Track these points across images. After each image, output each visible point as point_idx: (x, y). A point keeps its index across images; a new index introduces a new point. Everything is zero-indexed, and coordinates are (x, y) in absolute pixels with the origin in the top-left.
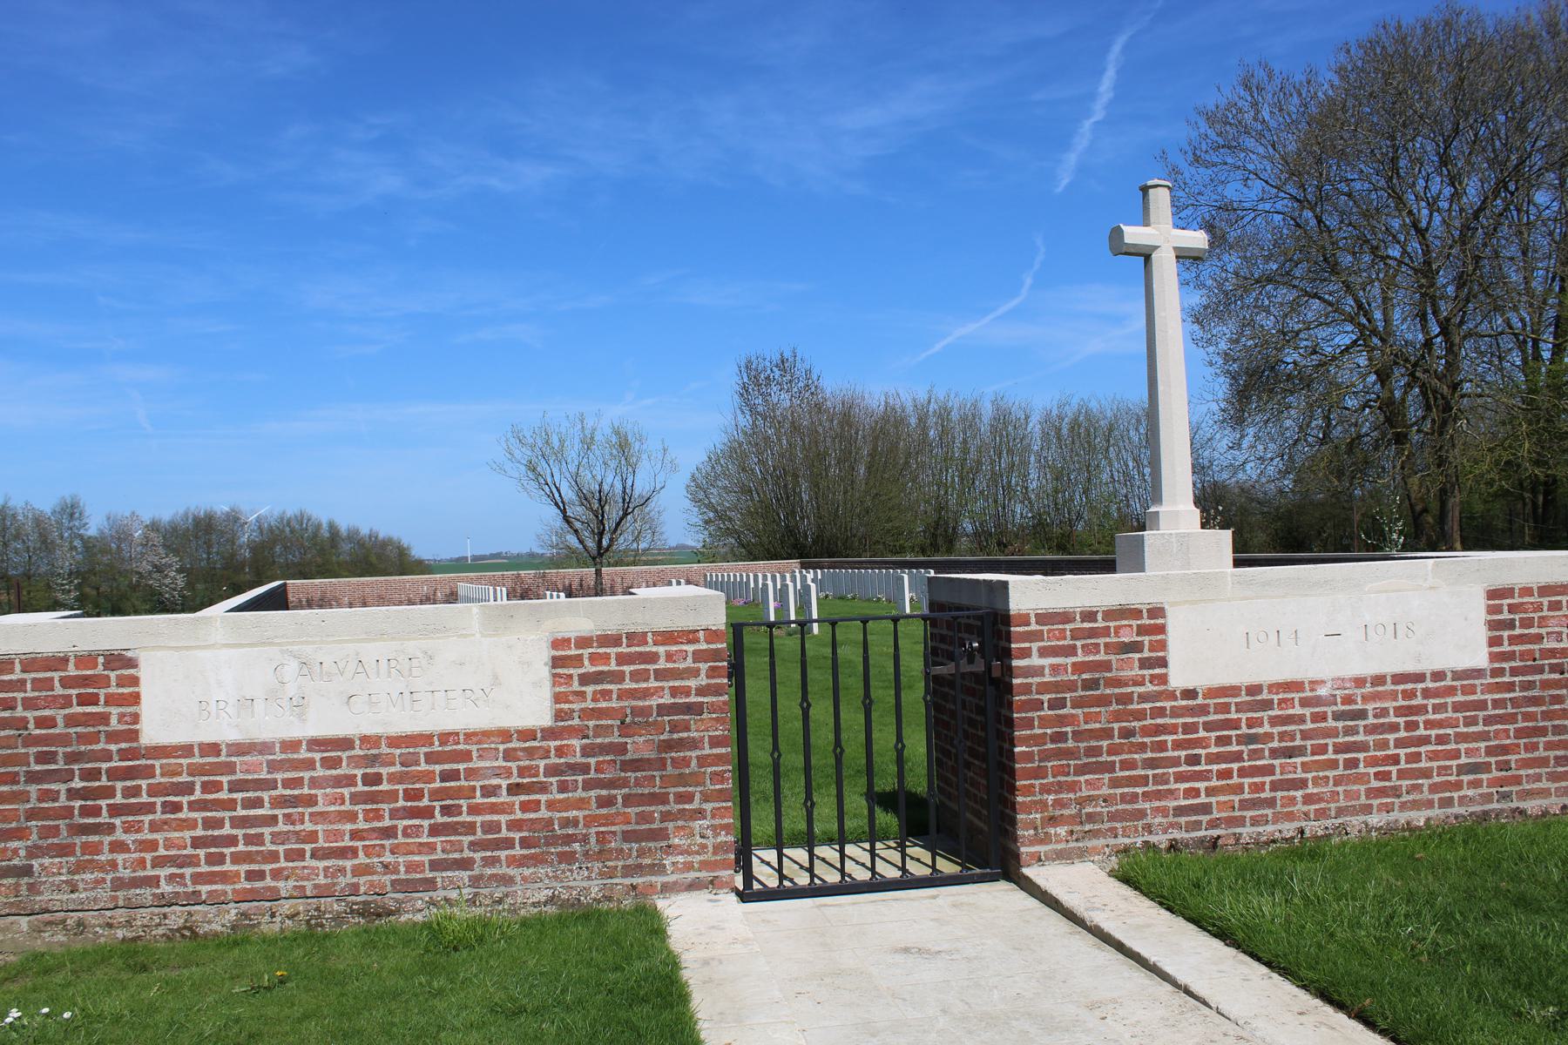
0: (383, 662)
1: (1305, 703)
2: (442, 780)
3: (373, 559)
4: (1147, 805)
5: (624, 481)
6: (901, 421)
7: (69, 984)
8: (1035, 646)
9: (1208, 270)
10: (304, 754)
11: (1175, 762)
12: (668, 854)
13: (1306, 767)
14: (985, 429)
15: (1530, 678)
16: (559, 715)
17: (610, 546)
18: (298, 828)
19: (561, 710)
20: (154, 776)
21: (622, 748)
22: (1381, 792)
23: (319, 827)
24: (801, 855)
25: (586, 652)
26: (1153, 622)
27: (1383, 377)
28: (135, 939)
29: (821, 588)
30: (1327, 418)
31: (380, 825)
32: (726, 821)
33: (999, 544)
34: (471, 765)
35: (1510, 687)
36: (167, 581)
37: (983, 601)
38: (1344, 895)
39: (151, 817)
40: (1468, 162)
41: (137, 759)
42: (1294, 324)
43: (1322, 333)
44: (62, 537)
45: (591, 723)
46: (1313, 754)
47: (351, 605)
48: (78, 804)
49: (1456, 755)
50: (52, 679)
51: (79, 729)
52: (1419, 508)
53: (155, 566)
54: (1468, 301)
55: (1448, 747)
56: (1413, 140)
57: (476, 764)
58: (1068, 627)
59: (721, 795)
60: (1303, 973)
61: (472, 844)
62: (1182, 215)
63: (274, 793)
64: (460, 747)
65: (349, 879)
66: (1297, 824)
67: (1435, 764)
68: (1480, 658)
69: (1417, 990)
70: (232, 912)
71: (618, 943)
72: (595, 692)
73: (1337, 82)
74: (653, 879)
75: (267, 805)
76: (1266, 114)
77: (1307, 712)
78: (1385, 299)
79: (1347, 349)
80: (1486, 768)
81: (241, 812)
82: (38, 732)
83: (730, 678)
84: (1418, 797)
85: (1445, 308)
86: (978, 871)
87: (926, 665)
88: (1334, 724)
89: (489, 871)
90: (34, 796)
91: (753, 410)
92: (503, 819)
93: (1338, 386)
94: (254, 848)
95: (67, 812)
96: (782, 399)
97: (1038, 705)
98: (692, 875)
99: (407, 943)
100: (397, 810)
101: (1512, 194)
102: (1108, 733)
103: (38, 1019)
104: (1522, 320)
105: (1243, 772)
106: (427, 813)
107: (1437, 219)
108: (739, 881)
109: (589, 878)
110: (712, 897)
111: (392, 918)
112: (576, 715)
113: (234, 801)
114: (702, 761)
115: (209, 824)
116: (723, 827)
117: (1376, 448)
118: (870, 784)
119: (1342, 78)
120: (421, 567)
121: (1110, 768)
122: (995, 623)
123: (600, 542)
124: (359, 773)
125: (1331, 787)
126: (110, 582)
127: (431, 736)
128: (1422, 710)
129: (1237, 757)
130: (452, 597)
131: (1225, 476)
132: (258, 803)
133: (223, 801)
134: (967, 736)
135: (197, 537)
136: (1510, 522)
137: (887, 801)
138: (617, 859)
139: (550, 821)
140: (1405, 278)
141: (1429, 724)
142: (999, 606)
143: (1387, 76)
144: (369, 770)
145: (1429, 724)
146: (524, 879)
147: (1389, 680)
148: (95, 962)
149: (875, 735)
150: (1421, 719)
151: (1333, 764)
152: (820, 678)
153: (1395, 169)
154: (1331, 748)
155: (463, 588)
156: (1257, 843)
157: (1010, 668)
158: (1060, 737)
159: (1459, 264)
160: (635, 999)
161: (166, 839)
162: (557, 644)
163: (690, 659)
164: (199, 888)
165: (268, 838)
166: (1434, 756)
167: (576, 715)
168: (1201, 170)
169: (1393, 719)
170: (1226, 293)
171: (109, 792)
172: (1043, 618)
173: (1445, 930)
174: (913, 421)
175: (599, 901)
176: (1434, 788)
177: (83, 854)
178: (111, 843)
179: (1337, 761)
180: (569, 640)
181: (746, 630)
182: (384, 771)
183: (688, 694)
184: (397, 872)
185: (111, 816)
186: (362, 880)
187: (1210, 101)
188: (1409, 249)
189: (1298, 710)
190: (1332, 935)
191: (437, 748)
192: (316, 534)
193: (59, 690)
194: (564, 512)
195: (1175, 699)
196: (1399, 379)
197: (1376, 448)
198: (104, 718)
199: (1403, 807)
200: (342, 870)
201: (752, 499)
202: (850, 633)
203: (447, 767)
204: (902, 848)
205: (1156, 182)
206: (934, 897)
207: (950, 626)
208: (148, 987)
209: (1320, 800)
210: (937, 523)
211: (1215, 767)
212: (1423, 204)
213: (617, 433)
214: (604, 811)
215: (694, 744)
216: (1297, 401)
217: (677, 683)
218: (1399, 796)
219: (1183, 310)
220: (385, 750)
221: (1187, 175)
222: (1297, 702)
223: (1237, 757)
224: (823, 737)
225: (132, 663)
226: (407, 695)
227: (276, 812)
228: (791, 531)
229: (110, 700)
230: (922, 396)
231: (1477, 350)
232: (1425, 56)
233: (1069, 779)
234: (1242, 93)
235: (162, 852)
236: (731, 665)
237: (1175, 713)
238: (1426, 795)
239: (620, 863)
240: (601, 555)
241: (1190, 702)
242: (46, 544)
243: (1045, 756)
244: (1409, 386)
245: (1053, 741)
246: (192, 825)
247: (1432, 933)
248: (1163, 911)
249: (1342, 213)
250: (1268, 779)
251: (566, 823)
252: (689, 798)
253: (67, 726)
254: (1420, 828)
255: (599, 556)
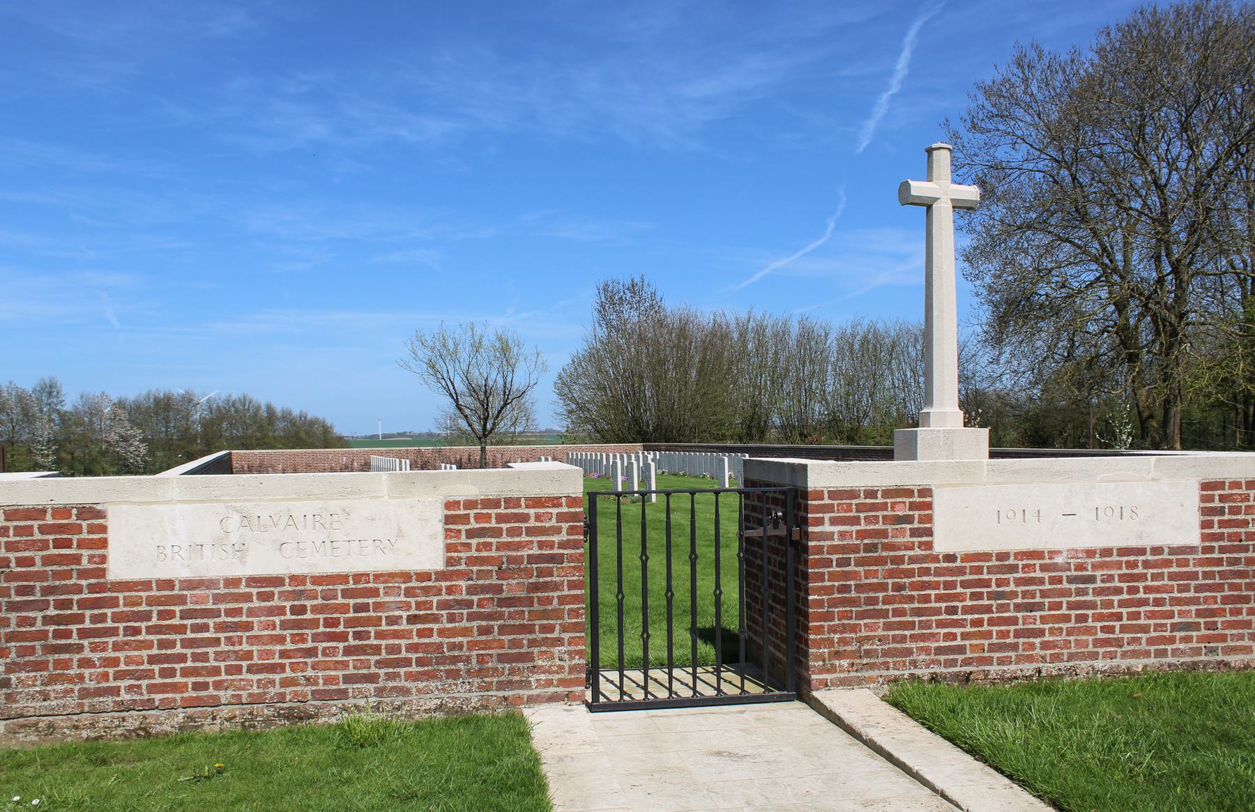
0: (310, 517)
1: (1044, 568)
2: (355, 611)
3: (303, 435)
4: (914, 645)
5: (505, 378)
6: (725, 336)
7: (38, 777)
8: (827, 516)
9: (978, 218)
10: (243, 589)
11: (937, 611)
12: (533, 673)
13: (1044, 620)
14: (792, 342)
15: (1236, 555)
16: (450, 561)
17: (492, 429)
18: (237, 648)
19: (451, 558)
20: (118, 606)
21: (499, 589)
22: (1106, 643)
23: (254, 648)
24: (637, 675)
25: (472, 512)
26: (922, 500)
27: (1121, 307)
28: (96, 739)
29: (659, 466)
30: (1072, 340)
31: (304, 646)
32: (579, 648)
33: (801, 435)
34: (378, 600)
35: (1219, 562)
36: (132, 449)
37: (787, 480)
38: (1074, 724)
39: (114, 639)
40: (1206, 129)
41: (103, 591)
42: (1047, 263)
43: (1071, 271)
44: (41, 411)
45: (475, 569)
46: (1050, 609)
47: (284, 471)
48: (51, 628)
49: (1170, 615)
50: (32, 527)
51: (54, 568)
52: (1145, 415)
53: (122, 437)
54: (1197, 245)
55: (1164, 608)
56: (1159, 110)
57: (382, 599)
58: (854, 502)
59: (576, 627)
60: (1039, 785)
61: (377, 662)
62: (960, 172)
63: (218, 620)
64: (370, 585)
65: (278, 689)
66: (1035, 665)
67: (1152, 622)
68: (1193, 537)
69: (1134, 805)
70: (180, 716)
71: (492, 743)
72: (478, 544)
73: (1096, 61)
74: (521, 692)
75: (212, 629)
76: (1034, 88)
77: (1046, 575)
78: (1126, 244)
79: (1091, 284)
80: (1196, 627)
81: (190, 635)
82: (19, 569)
83: (585, 535)
84: (1137, 648)
85: (1177, 251)
86: (777, 692)
87: (740, 529)
88: (1068, 586)
89: (390, 684)
90: (13, 622)
91: (608, 324)
92: (403, 642)
93: (1082, 314)
94: (200, 664)
95: (43, 635)
96: (632, 316)
97: (828, 563)
98: (551, 690)
99: (323, 741)
100: (318, 634)
101: (1243, 155)
102: (882, 587)
103: (10, 806)
104: (1244, 262)
105: (992, 622)
106: (342, 637)
107: (1175, 176)
108: (588, 695)
109: (470, 691)
110: (567, 707)
111: (311, 721)
112: (463, 561)
113: (185, 626)
114: (562, 600)
115: (162, 644)
116: (577, 652)
117: (1112, 365)
118: (694, 622)
119: (1101, 58)
120: (341, 442)
121: (884, 614)
122: (796, 497)
123: (485, 425)
124: (288, 604)
125: (1064, 637)
126: (81, 447)
127: (347, 576)
128: (1142, 577)
129: (988, 609)
130: (366, 467)
131: (985, 385)
132: (205, 628)
133: (175, 626)
134: (771, 585)
135: (156, 414)
136: (1224, 427)
137: (707, 635)
138: (493, 676)
139: (440, 645)
140: (1144, 226)
141: (1148, 589)
142: (799, 484)
143: (1140, 55)
144: (296, 603)
145: (1148, 589)
146: (419, 691)
147: (1115, 552)
148: (62, 758)
149: (699, 583)
150: (1141, 585)
151: (1067, 618)
152: (656, 537)
153: (1142, 135)
154: (1064, 605)
155: (375, 460)
156: (1002, 679)
157: (807, 533)
158: (846, 589)
159: (1192, 214)
160: (504, 788)
161: (127, 657)
162: (449, 505)
163: (554, 519)
164: (153, 696)
165: (212, 656)
166: (1151, 615)
167: (463, 561)
168: (978, 135)
169: (1117, 584)
170: (992, 238)
171: (79, 619)
172: (834, 494)
173: (1158, 757)
174: (736, 336)
175: (477, 709)
176: (1151, 641)
177: (55, 669)
178: (79, 660)
179: (1069, 616)
180: (458, 502)
181: (599, 498)
182: (308, 603)
183: (552, 547)
184: (316, 683)
185: (80, 638)
186: (288, 690)
187: (989, 76)
188: (1149, 202)
189: (1038, 574)
190: (1063, 756)
191: (351, 585)
192: (256, 415)
193: (37, 536)
194: (457, 401)
195: (939, 561)
196: (1134, 309)
197: (1112, 365)
198: (77, 559)
199: (1124, 655)
200: (272, 682)
201: (606, 395)
202: (681, 502)
203: (359, 601)
204: (717, 672)
205: (940, 145)
206: (742, 712)
207: (760, 499)
208: (106, 777)
209: (1055, 647)
210: (752, 418)
211: (969, 617)
212: (1164, 164)
213: (500, 339)
214: (483, 638)
215: (557, 587)
216: (1047, 326)
217: (543, 538)
218: (1121, 646)
219: (956, 250)
220: (309, 586)
221: (965, 139)
222: (1037, 568)
223: (988, 609)
224: (657, 583)
225: (101, 515)
226: (328, 543)
227: (219, 635)
228: (636, 421)
229: (82, 544)
230: (743, 316)
231: (1203, 286)
232: (1175, 38)
233: (851, 622)
234: (1016, 71)
235: (123, 667)
236: (587, 525)
237: (938, 572)
238: (1144, 646)
239: (495, 679)
240: (485, 436)
241: (951, 565)
242: (28, 416)
243: (833, 603)
244: (1142, 315)
245: (839, 592)
246: (149, 645)
247: (1148, 759)
248: (924, 730)
249: (1094, 172)
250: (1012, 628)
251: (453, 647)
252: (551, 629)
253: (44, 564)
254: (1138, 673)
255: (483, 437)
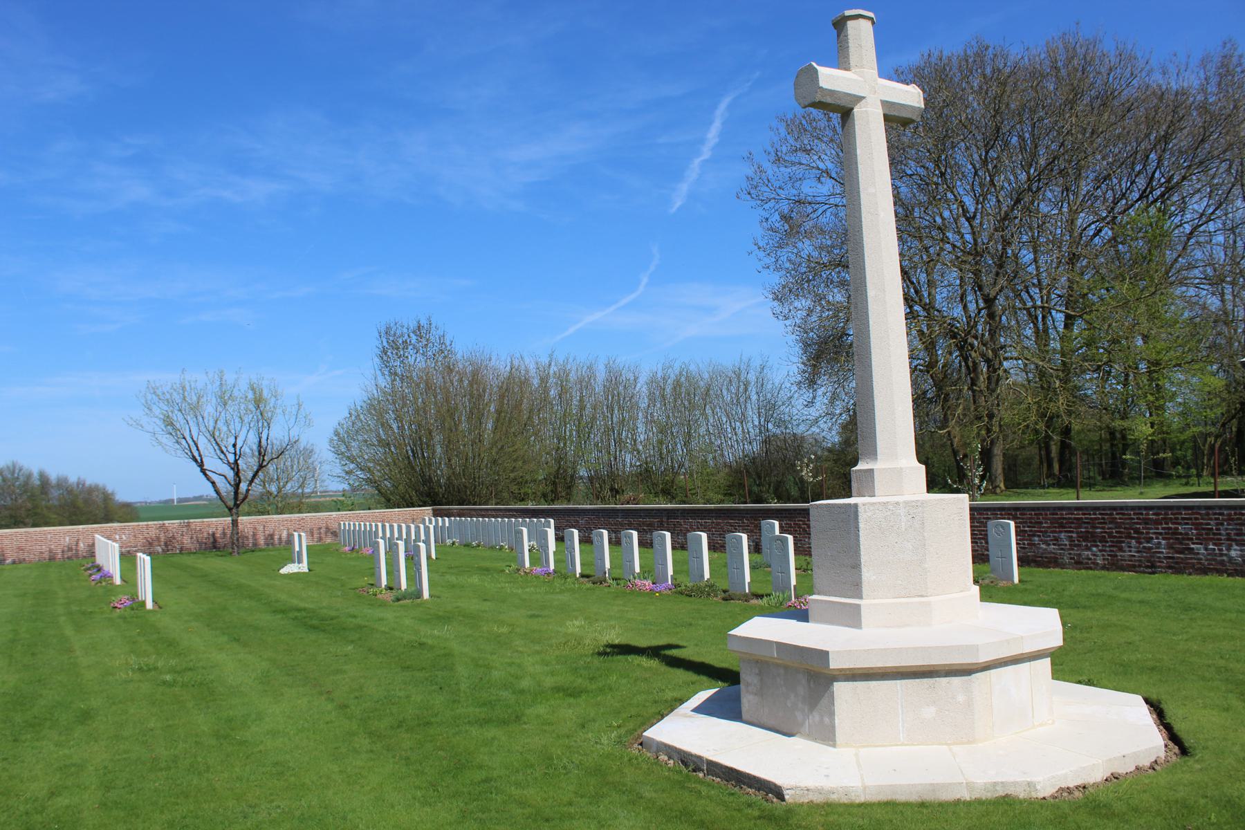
3: (80, 503)
5: (260, 434)
6: (525, 382)
14: (599, 389)
33: (612, 489)
96: (418, 362)
131: (802, 428)
174: (536, 382)
192: (26, 483)
210: (556, 477)
221: (770, 172)
228: (427, 481)
240: (237, 506)
